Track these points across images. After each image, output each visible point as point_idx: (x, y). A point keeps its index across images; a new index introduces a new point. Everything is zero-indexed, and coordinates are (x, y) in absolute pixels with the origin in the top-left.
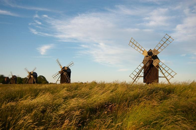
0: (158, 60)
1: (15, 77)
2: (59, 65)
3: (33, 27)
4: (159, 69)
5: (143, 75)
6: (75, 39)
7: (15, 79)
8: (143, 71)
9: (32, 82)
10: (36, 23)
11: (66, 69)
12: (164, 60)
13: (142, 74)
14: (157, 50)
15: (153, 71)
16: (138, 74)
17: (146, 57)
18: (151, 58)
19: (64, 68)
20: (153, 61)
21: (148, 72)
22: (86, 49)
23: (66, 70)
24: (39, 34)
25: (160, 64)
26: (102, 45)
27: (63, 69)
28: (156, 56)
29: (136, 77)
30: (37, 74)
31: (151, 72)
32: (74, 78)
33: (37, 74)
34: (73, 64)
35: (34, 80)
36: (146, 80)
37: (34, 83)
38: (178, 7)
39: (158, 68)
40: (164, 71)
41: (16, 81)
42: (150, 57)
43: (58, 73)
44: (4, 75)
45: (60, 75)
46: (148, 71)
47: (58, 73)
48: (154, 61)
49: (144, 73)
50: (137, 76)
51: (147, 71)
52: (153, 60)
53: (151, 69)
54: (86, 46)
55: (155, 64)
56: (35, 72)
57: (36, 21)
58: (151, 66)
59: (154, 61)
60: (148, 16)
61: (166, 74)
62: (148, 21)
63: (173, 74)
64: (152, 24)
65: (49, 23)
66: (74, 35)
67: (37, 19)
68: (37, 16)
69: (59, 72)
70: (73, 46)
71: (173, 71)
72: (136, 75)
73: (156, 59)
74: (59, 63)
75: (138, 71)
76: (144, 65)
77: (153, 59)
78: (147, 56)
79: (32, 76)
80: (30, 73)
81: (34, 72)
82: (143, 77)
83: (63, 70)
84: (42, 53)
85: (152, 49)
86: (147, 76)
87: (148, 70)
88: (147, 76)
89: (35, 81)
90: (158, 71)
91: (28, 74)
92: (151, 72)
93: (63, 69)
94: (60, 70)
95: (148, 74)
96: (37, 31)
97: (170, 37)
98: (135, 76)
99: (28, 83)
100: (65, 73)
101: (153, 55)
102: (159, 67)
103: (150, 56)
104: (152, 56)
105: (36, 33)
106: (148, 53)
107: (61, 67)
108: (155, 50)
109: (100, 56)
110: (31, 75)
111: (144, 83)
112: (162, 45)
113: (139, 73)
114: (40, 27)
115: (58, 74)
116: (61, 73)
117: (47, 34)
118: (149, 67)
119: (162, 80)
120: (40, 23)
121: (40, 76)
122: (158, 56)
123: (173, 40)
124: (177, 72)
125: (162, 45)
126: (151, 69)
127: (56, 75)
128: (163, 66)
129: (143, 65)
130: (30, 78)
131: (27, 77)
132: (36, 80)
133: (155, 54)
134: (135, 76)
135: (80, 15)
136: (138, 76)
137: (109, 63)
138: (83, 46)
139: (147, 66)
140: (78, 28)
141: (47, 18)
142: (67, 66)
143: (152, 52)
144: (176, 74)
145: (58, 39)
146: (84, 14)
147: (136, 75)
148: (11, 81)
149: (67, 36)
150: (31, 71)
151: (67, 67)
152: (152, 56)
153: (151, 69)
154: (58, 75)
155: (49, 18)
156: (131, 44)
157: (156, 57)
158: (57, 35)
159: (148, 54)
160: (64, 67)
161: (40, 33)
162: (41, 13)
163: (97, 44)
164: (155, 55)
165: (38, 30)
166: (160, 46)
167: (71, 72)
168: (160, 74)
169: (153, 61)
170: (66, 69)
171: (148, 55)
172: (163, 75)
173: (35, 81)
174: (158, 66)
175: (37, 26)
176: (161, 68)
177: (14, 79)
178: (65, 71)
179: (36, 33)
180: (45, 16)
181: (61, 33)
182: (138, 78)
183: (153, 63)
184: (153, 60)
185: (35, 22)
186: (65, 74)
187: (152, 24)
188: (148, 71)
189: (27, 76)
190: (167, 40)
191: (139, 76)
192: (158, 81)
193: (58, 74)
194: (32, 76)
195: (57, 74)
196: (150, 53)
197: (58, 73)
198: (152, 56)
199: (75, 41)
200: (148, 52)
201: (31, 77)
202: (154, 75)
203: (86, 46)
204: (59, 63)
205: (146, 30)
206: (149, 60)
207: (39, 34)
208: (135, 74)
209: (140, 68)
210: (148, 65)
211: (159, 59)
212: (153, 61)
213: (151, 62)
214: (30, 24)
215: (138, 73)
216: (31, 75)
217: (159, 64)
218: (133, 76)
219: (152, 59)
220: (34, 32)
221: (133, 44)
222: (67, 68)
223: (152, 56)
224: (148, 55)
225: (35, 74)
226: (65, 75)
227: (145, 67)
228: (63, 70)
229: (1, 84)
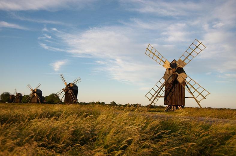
0: (184, 74)
1: (19, 95)
2: (63, 81)
3: (42, 41)
4: (186, 86)
5: (163, 95)
6: (90, 55)
7: (20, 97)
8: (164, 89)
9: (36, 101)
10: (45, 37)
11: (72, 86)
12: (191, 76)
13: (162, 94)
14: (183, 61)
15: (177, 90)
16: (157, 94)
17: (168, 70)
18: (175, 72)
19: (69, 84)
20: (178, 75)
21: (170, 91)
22: (103, 66)
23: (71, 87)
24: (49, 49)
25: (188, 80)
26: (119, 60)
27: (69, 86)
28: (182, 69)
29: (154, 98)
30: (41, 91)
31: (174, 91)
32: (82, 98)
33: (42, 92)
34: (80, 81)
35: (37, 100)
36: (168, 101)
37: (38, 102)
38: (196, 22)
39: (184, 85)
40: (192, 90)
41: (20, 100)
42: (174, 70)
43: (62, 91)
44: (10, 93)
45: (64, 93)
46: (171, 89)
47: (62, 91)
48: (179, 75)
49: (166, 91)
50: (155, 96)
51: (169, 89)
52: (177, 74)
53: (174, 87)
54: (102, 63)
55: (180, 80)
56: (40, 90)
57: (45, 35)
58: (175, 82)
59: (179, 75)
60: (166, 31)
61: (196, 94)
62: (167, 36)
63: (204, 94)
64: (171, 39)
65: (59, 37)
66: (88, 50)
67: (45, 32)
68: (45, 29)
69: (62, 89)
70: (87, 62)
71: (204, 90)
72: (154, 95)
73: (182, 73)
74: (63, 79)
75: (156, 89)
76: (165, 81)
77: (177, 72)
78: (169, 69)
79: (35, 94)
80: (34, 90)
81: (38, 89)
82: (164, 98)
83: (68, 88)
84: (56, 70)
85: (177, 60)
86: (169, 96)
87: (170, 88)
88: (169, 96)
89: (39, 100)
90: (184, 89)
91: (31, 92)
92: (174, 91)
93: (69, 86)
94: (64, 87)
95: (171, 93)
96: (47, 46)
97: (201, 43)
98: (153, 96)
99: (31, 103)
100: (70, 92)
101: (178, 67)
102: (186, 84)
103: (173, 68)
104: (176, 70)
105: (46, 48)
106: (171, 65)
107: (66, 84)
108: (180, 61)
109: (117, 74)
110: (35, 92)
111: (166, 106)
112: (187, 58)
113: (158, 92)
114: (49, 41)
115: (62, 92)
116: (66, 91)
117: (58, 49)
118: (172, 84)
119: (189, 103)
120: (50, 37)
121: (53, 94)
122: (184, 68)
123: (193, 57)
124: (211, 91)
125: (187, 58)
126: (175, 86)
127: (60, 94)
128: (192, 83)
129: (163, 81)
130: (34, 96)
131: (30, 95)
132: (39, 98)
133: (181, 67)
134: (153, 96)
135: (91, 28)
136: (157, 96)
137: (129, 80)
138: (99, 62)
139: (170, 82)
140: (92, 42)
141: (56, 31)
142: (73, 83)
143: (177, 63)
144: (209, 93)
145: (70, 54)
146: (95, 28)
147: (154, 95)
148: (23, 100)
149: (80, 52)
150: (34, 88)
151: (73, 84)
152: (177, 68)
153: (174, 87)
154: (61, 94)
155: (59, 32)
156: (148, 52)
157: (181, 71)
158: (69, 50)
159: (171, 67)
160: (70, 83)
161: (51, 47)
162: (50, 26)
163: (114, 60)
164: (181, 68)
165: (48, 44)
166: (184, 59)
167: (78, 90)
168: (187, 94)
169: (178, 75)
170: (71, 86)
171: (171, 68)
172: (191, 95)
173: (39, 100)
174: (184, 83)
175: (47, 41)
176: (188, 85)
177: (18, 97)
178: (70, 88)
179: (46, 48)
180: (55, 29)
181: (73, 48)
182: (158, 98)
183: (178, 78)
184: (177, 74)
185: (44, 36)
186: (72, 91)
187: (171, 39)
188: (171, 89)
189: (30, 94)
190: (197, 47)
191: (159, 96)
192: (184, 104)
193: (62, 92)
194: (35, 94)
195: (60, 92)
196: (173, 65)
197: (62, 91)
198: (176, 70)
199: (90, 57)
200: (171, 63)
201: (34, 96)
202: (179, 94)
203: (102, 63)
204: (63, 79)
205: (166, 46)
206: (172, 75)
207: (49, 49)
208: (153, 92)
209: (160, 85)
210: (170, 81)
211: (185, 73)
212: (177, 75)
213: (175, 77)
214: (39, 38)
215: (156, 92)
216: (35, 92)
217: (185, 80)
218: (150, 96)
219: (176, 73)
220: (44, 46)
221: (151, 53)
222: (72, 85)
223: (177, 68)
224: (171, 68)
225: (39, 93)
226: (70, 93)
227: (166, 84)
228: (68, 88)
229: (6, 102)
